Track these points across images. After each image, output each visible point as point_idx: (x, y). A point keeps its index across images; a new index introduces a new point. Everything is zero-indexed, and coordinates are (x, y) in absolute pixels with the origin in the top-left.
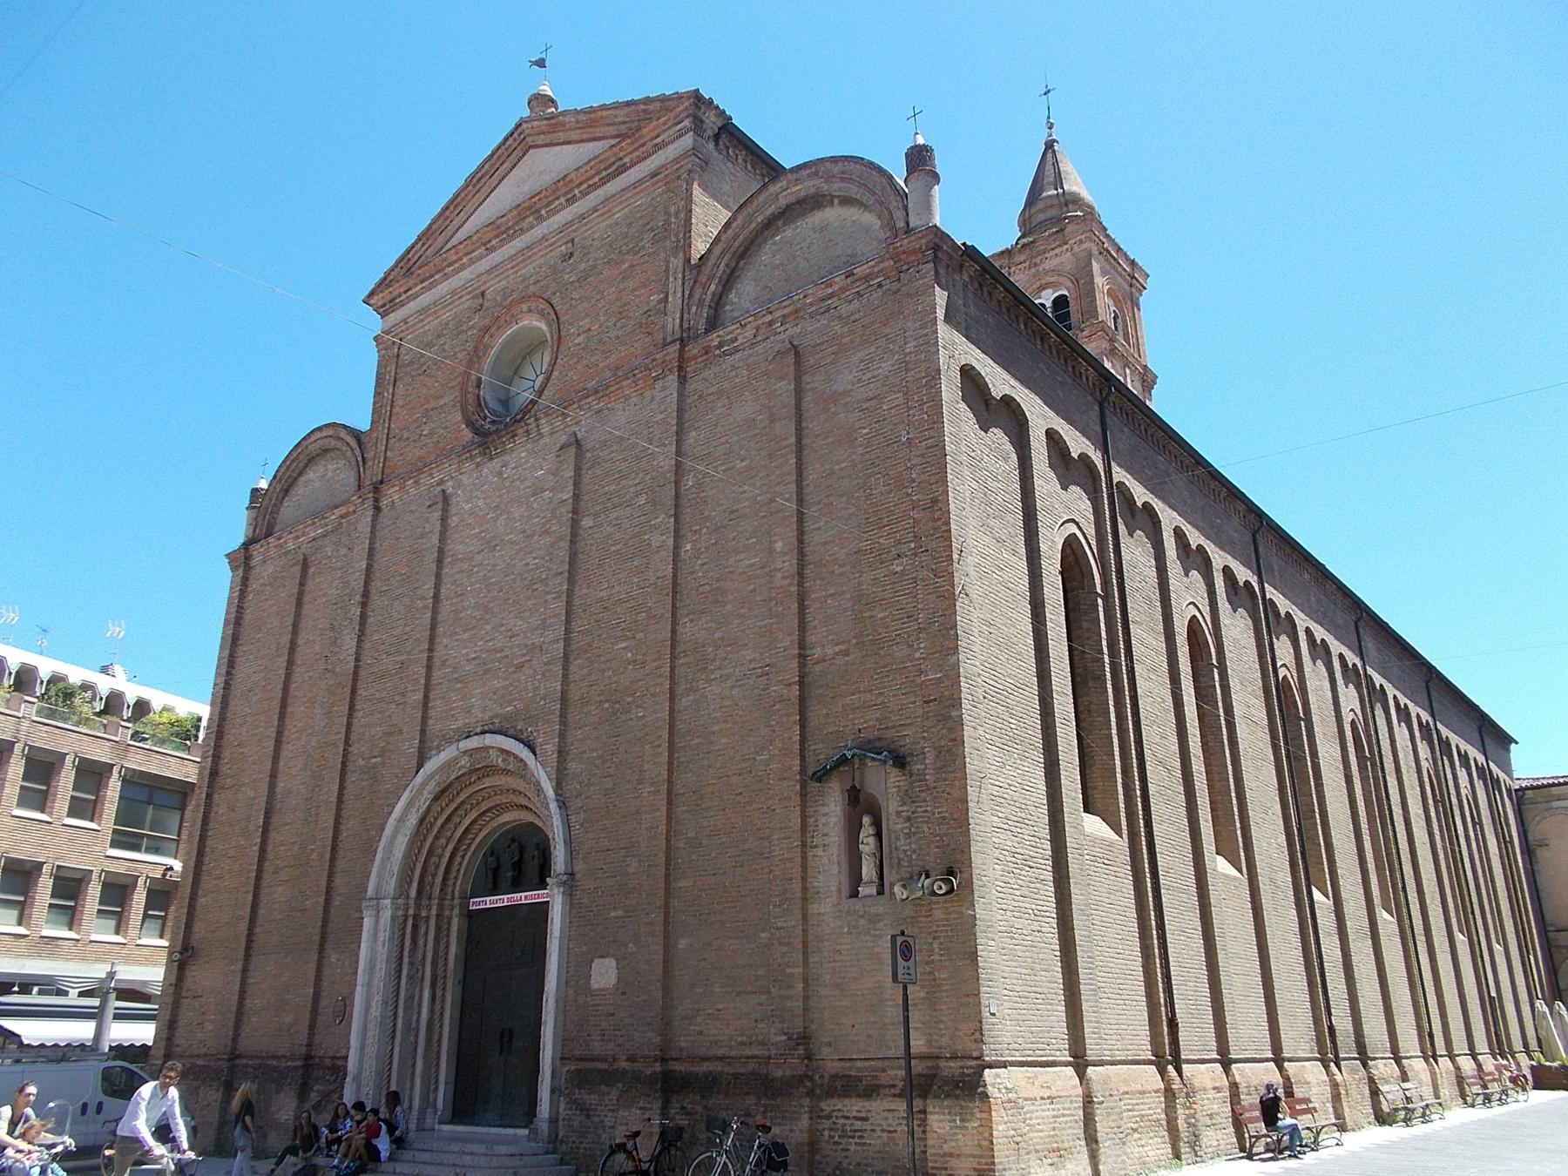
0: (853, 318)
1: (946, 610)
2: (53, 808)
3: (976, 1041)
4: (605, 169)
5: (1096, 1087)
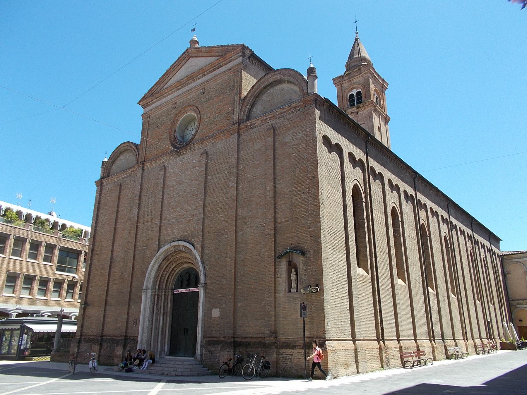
0: (291, 120)
1: (317, 210)
2: (39, 259)
3: (323, 333)
5: (358, 347)
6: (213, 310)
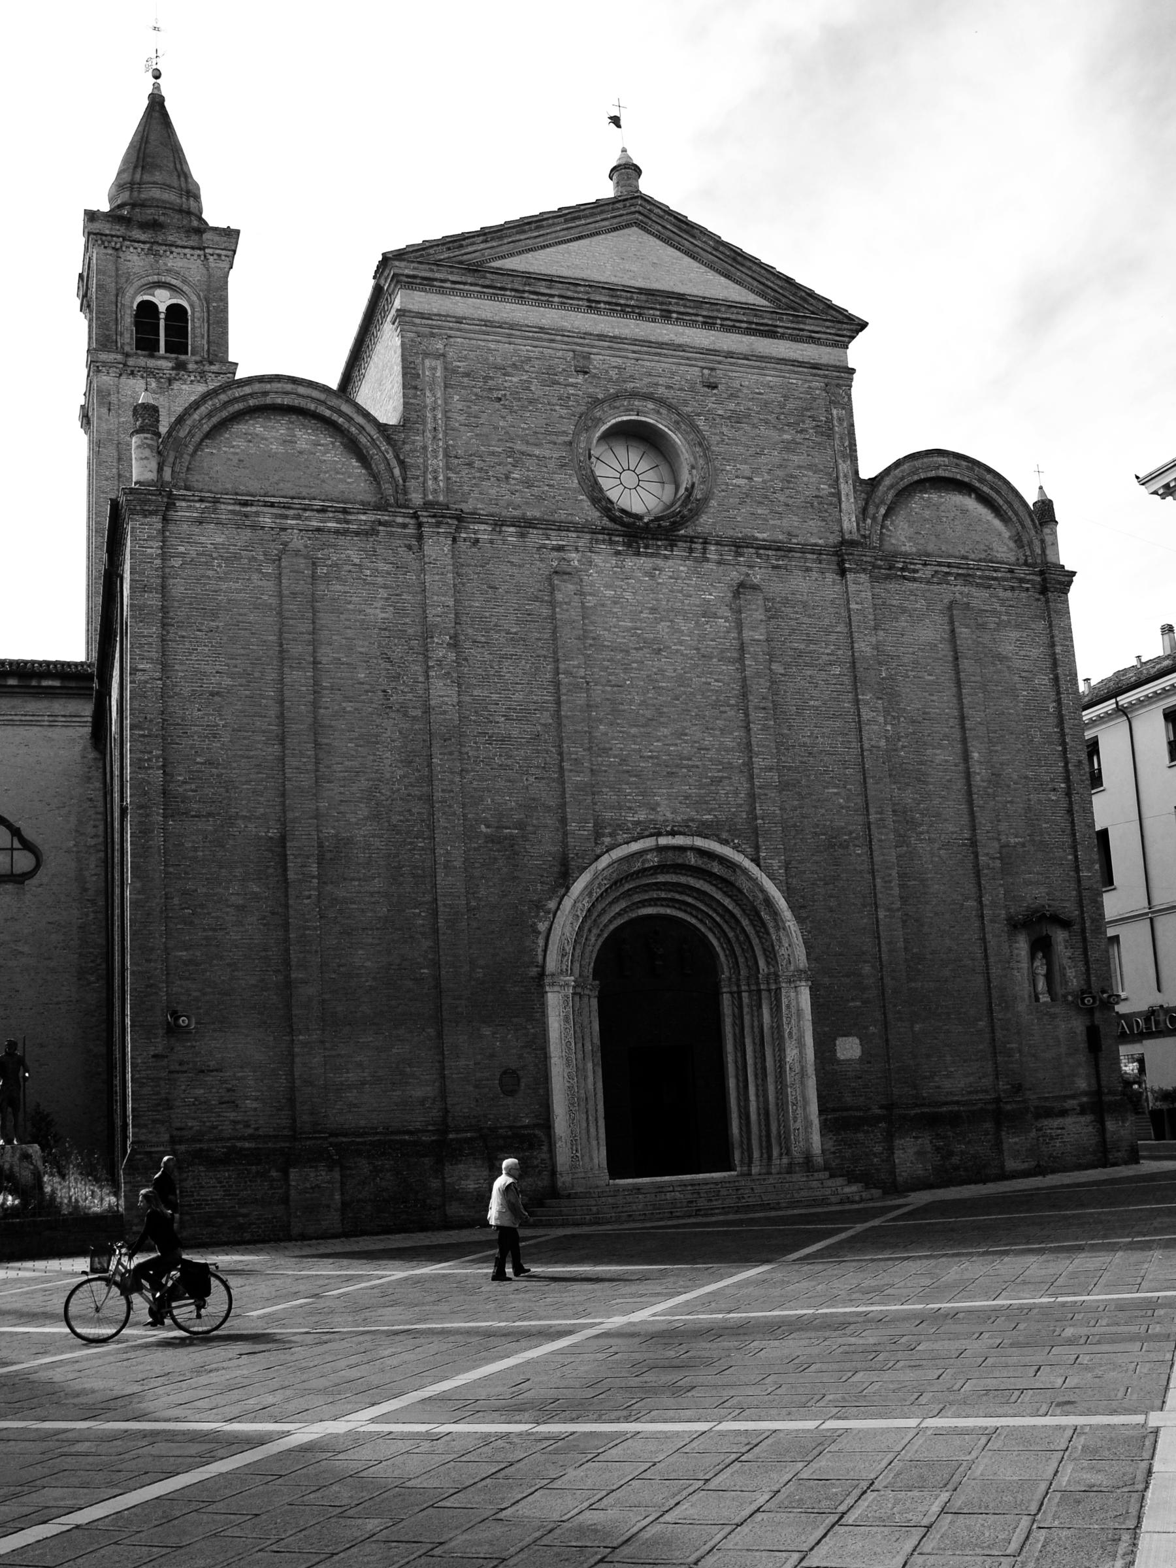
4: (757, 324)
6: (837, 1042)
